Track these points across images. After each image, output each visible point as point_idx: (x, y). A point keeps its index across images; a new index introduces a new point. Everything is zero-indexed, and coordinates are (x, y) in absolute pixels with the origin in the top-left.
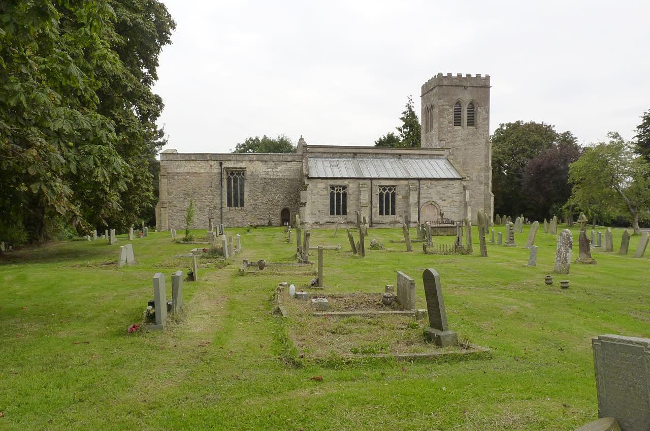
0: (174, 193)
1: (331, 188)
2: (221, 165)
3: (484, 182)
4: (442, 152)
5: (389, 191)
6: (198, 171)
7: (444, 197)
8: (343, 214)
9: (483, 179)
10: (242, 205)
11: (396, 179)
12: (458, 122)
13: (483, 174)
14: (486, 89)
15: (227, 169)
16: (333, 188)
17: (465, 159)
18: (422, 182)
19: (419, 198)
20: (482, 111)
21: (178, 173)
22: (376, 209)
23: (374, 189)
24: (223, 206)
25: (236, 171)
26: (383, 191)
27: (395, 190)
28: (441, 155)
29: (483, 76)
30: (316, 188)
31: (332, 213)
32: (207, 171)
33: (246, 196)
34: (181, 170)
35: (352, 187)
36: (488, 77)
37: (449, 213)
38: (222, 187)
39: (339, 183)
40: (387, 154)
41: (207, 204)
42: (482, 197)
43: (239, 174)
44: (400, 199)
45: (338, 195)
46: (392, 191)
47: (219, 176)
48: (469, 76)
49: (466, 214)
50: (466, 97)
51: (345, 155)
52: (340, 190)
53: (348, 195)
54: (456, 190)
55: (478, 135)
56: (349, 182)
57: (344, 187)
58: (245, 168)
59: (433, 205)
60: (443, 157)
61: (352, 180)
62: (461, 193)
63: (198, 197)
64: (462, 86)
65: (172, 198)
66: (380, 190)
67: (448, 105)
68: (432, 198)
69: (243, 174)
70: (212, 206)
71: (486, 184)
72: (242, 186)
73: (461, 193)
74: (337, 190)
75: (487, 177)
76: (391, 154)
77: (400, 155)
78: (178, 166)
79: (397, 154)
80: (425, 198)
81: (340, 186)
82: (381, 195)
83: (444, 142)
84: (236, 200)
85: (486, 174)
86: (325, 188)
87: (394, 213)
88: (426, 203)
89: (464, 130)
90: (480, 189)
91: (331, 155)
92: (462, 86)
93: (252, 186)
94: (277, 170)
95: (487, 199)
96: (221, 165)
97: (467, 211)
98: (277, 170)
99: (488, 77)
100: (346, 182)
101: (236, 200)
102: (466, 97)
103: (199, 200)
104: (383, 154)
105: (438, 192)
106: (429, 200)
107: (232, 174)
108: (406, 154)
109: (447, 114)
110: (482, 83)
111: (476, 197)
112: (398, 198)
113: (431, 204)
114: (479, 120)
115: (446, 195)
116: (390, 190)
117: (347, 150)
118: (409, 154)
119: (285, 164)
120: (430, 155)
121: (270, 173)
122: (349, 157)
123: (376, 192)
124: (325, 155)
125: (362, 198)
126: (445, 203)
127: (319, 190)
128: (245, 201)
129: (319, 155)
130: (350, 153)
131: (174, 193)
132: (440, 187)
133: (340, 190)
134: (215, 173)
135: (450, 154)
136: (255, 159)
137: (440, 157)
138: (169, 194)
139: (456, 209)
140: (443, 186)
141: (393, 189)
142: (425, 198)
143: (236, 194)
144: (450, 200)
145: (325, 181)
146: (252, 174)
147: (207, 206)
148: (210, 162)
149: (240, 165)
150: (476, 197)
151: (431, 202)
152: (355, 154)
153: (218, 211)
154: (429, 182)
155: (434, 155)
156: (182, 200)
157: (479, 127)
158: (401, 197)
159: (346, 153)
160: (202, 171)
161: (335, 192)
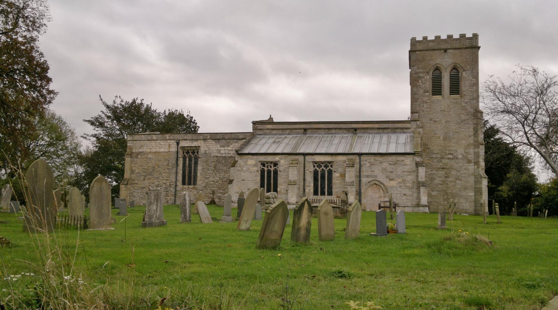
0: (137, 171)
1: (261, 164)
2: (178, 144)
3: (473, 161)
4: (408, 125)
5: (324, 168)
6: (158, 150)
7: (392, 176)
8: (328, 195)
9: (471, 157)
10: (195, 184)
11: (332, 154)
12: (437, 90)
13: (471, 151)
14: (474, 50)
15: (183, 148)
16: (263, 165)
17: (446, 133)
18: (363, 158)
19: (360, 176)
20: (468, 76)
21: (141, 152)
22: (310, 189)
23: (307, 165)
24: (178, 184)
25: (190, 150)
26: (318, 169)
27: (331, 166)
28: (406, 128)
29: (469, 35)
30: (246, 164)
32: (165, 150)
33: (199, 174)
34: (144, 149)
35: (283, 162)
36: (475, 36)
37: (399, 195)
38: (177, 166)
39: (270, 159)
40: (341, 129)
41: (164, 182)
42: (472, 180)
43: (193, 153)
44: (337, 177)
45: (269, 172)
46: (328, 168)
47: (175, 155)
48: (450, 37)
49: (419, 198)
50: (446, 62)
51: (294, 131)
52: (271, 167)
53: (279, 172)
54: (407, 168)
56: (280, 158)
57: (276, 164)
58: (199, 147)
59: (377, 184)
60: (410, 131)
61: (283, 156)
62: (414, 171)
63: (156, 175)
64: (441, 49)
65: (135, 175)
66: (314, 166)
68: (376, 176)
69: (198, 152)
70: (168, 184)
71: (477, 163)
72: (196, 164)
73: (414, 171)
74: (267, 167)
75: (477, 155)
76: (345, 129)
77: (356, 130)
78: (142, 146)
79: (352, 129)
80: (367, 176)
81: (271, 163)
82: (316, 173)
83: (417, 114)
84: (190, 178)
85: (476, 150)
86: (255, 165)
87: (330, 194)
88: (369, 182)
89: (446, 99)
90: (468, 170)
91: (280, 132)
92: (441, 49)
93: (204, 164)
94: (229, 148)
95: (478, 181)
96: (178, 144)
97: (419, 193)
98: (229, 148)
99: (475, 36)
100: (277, 158)
101: (190, 178)
102: (446, 62)
103: (158, 178)
104: (335, 129)
105: (384, 170)
106: (373, 179)
107: (188, 152)
108: (363, 128)
109: (422, 82)
110: (467, 44)
111: (463, 179)
112: (336, 175)
113: (376, 184)
114: (465, 86)
115: (394, 173)
116: (326, 166)
117: (322, 126)
118: (367, 128)
119: (236, 142)
120: (392, 129)
121: (222, 152)
122: (299, 133)
123: (310, 168)
124: (274, 132)
125: (290, 176)
126: (393, 183)
127: (250, 167)
128: (198, 179)
129: (268, 131)
131: (137, 171)
132: (386, 163)
133: (271, 167)
134: (172, 152)
135: (418, 127)
136: (208, 137)
137: (405, 130)
138: (132, 172)
139: (408, 190)
140: (391, 163)
141: (330, 165)
142: (367, 176)
143: (190, 172)
144: (400, 180)
145: (255, 157)
146: (205, 153)
147: (164, 183)
148: (169, 141)
149: (195, 144)
150: (463, 179)
151: (374, 182)
152: (305, 130)
153: (172, 189)
154: (372, 158)
155: (397, 128)
156: (142, 177)
157: (465, 95)
158: (338, 175)
159: (296, 129)
160: (162, 150)
161: (266, 169)
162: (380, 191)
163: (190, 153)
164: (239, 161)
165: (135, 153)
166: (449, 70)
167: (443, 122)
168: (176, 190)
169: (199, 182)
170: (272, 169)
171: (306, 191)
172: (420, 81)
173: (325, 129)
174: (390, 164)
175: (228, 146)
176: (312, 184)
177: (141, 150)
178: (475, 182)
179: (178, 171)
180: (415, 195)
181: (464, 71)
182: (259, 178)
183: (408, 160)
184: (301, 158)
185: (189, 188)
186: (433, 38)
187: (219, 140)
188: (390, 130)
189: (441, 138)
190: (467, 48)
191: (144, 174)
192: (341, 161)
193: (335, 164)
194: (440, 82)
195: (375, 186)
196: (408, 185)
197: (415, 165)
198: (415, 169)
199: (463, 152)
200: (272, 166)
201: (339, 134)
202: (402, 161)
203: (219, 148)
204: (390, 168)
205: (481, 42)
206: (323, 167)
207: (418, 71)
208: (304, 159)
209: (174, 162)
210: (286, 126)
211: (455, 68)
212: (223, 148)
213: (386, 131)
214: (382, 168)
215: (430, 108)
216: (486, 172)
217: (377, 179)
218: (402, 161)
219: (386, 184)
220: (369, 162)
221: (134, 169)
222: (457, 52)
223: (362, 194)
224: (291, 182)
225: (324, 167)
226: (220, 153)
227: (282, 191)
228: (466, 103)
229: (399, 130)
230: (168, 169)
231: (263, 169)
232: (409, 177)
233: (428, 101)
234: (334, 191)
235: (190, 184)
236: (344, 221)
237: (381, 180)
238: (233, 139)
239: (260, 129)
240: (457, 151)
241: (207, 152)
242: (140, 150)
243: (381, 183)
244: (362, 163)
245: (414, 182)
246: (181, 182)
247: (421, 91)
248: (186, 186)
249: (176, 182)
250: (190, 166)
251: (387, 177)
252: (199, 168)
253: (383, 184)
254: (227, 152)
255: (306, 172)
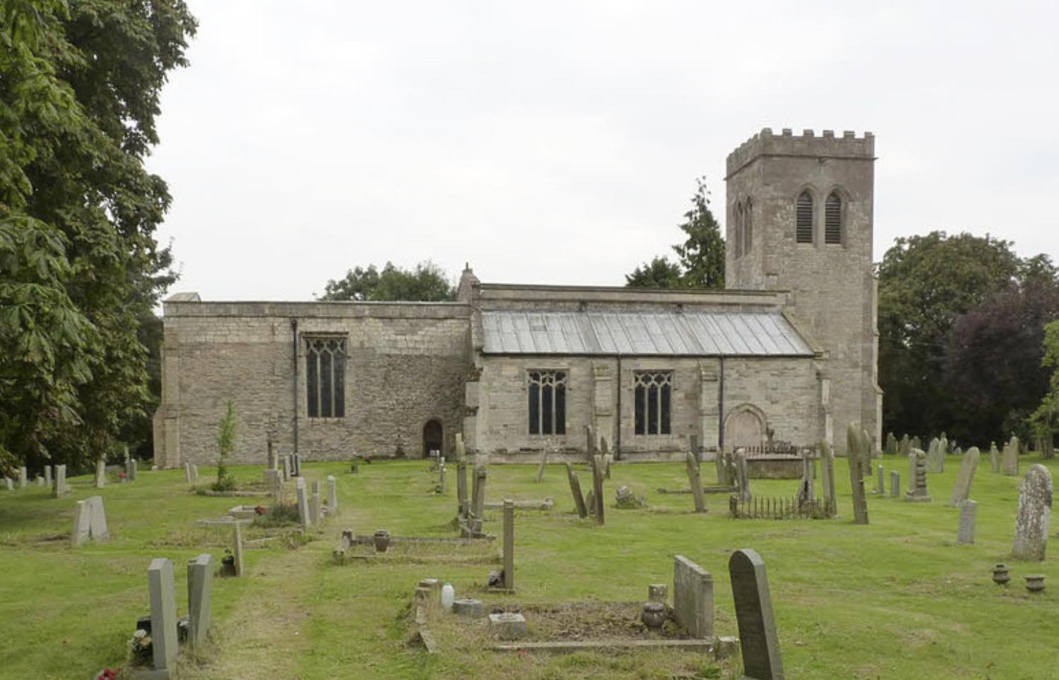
0: (194, 386)
1: (531, 375)
3: (861, 364)
4: (770, 299)
5: (656, 383)
6: (244, 339)
7: (776, 395)
9: (858, 356)
10: (340, 413)
11: (671, 357)
12: (804, 234)
15: (308, 336)
16: (535, 375)
17: (819, 313)
18: (727, 363)
21: (201, 344)
22: (629, 422)
23: (624, 377)
24: (300, 414)
27: (669, 379)
28: (769, 305)
29: (860, 135)
30: (499, 375)
31: (534, 430)
33: (348, 394)
34: (209, 337)
35: (577, 373)
36: (869, 138)
38: (296, 373)
39: (548, 365)
40: (653, 303)
41: (266, 410)
42: (857, 396)
43: (332, 345)
44: (680, 399)
45: (547, 391)
46: (663, 383)
48: (828, 135)
50: (823, 180)
51: (561, 304)
53: (567, 392)
54: (800, 381)
55: (849, 262)
56: (570, 364)
57: (560, 375)
58: (347, 333)
59: (752, 412)
60: (774, 309)
61: (576, 360)
64: (813, 157)
66: (637, 380)
67: (784, 198)
68: (749, 397)
69: (342, 346)
70: (276, 415)
71: (867, 368)
72: (340, 372)
73: (812, 387)
74: (544, 381)
75: (867, 353)
77: (680, 305)
79: (673, 303)
80: (734, 397)
81: (552, 372)
82: (639, 392)
83: (775, 278)
84: (326, 401)
85: (867, 345)
86: (519, 377)
87: (666, 430)
88: (737, 407)
89: (817, 253)
90: (853, 379)
91: (532, 306)
92: (813, 157)
94: (416, 338)
95: (867, 399)
98: (416, 338)
99: (869, 138)
100: (563, 364)
101: (326, 401)
102: (823, 180)
103: (248, 403)
104: (643, 302)
105: (763, 385)
106: (743, 402)
107: (319, 345)
108: (693, 303)
110: (857, 151)
112: (677, 397)
113: (748, 411)
114: (851, 229)
116: (659, 379)
118: (700, 303)
119: (432, 325)
120: (744, 305)
121: (400, 345)
122: (570, 310)
123: (630, 384)
124: (519, 306)
126: (777, 409)
128: (347, 404)
129: (505, 304)
130: (573, 301)
132: (766, 373)
135: (788, 303)
136: (367, 313)
137: (767, 309)
138: (183, 389)
139: (800, 421)
142: (734, 397)
144: (788, 403)
145: (519, 360)
147: (266, 414)
148: (271, 319)
149: (334, 327)
151: (747, 407)
152: (583, 303)
154: (742, 364)
156: (210, 401)
159: (564, 301)
160: (254, 339)
161: (541, 385)
162: (754, 421)
163: (326, 347)
164: (486, 369)
165: (186, 345)
166: (825, 197)
167: (816, 292)
168: (296, 427)
169: (348, 411)
170: (554, 384)
171: (622, 426)
172: (778, 215)
173: (623, 302)
174: (772, 375)
175: (414, 333)
176: (633, 414)
177: (202, 339)
178: (863, 401)
179: (299, 386)
180: (815, 428)
181: (850, 200)
182: (526, 404)
183: (803, 366)
184: (612, 364)
185: (326, 422)
186: (801, 134)
187: (391, 318)
188: (741, 308)
189: (813, 322)
190: (856, 159)
191: (214, 392)
192: (686, 369)
193: (677, 375)
194: (810, 217)
195: (746, 414)
196: (801, 411)
197: (814, 376)
198: (816, 382)
199: (846, 348)
200: (554, 378)
201: (650, 312)
202: (794, 369)
203: (393, 337)
204: (772, 381)
205: (879, 150)
206: (326, 347)
207: (776, 194)
208: (619, 366)
209: (287, 365)
210: (544, 295)
211: (833, 194)
212: (403, 338)
213: (734, 308)
214: (759, 382)
215: (794, 266)
216: (880, 384)
217: (750, 402)
218: (794, 369)
219: (765, 411)
220: (737, 372)
221: (185, 381)
222: (841, 163)
223: (725, 430)
224: (600, 411)
225: (656, 380)
226: (396, 348)
227: (577, 428)
228: (853, 260)
229: (757, 309)
230: (273, 382)
231: (535, 385)
232: (804, 397)
233: (792, 253)
234: (673, 424)
235: (329, 416)
236: (93, 476)
237: (755, 403)
238: (425, 318)
239: (490, 300)
240: (837, 346)
241: (366, 345)
242: (198, 339)
243: (758, 409)
244: (725, 372)
245: (811, 407)
246: (306, 411)
247: (780, 234)
248: (320, 420)
249: (295, 411)
250: (325, 375)
251: (767, 398)
252: (349, 380)
253: (761, 411)
254: (411, 345)
255: (622, 389)
